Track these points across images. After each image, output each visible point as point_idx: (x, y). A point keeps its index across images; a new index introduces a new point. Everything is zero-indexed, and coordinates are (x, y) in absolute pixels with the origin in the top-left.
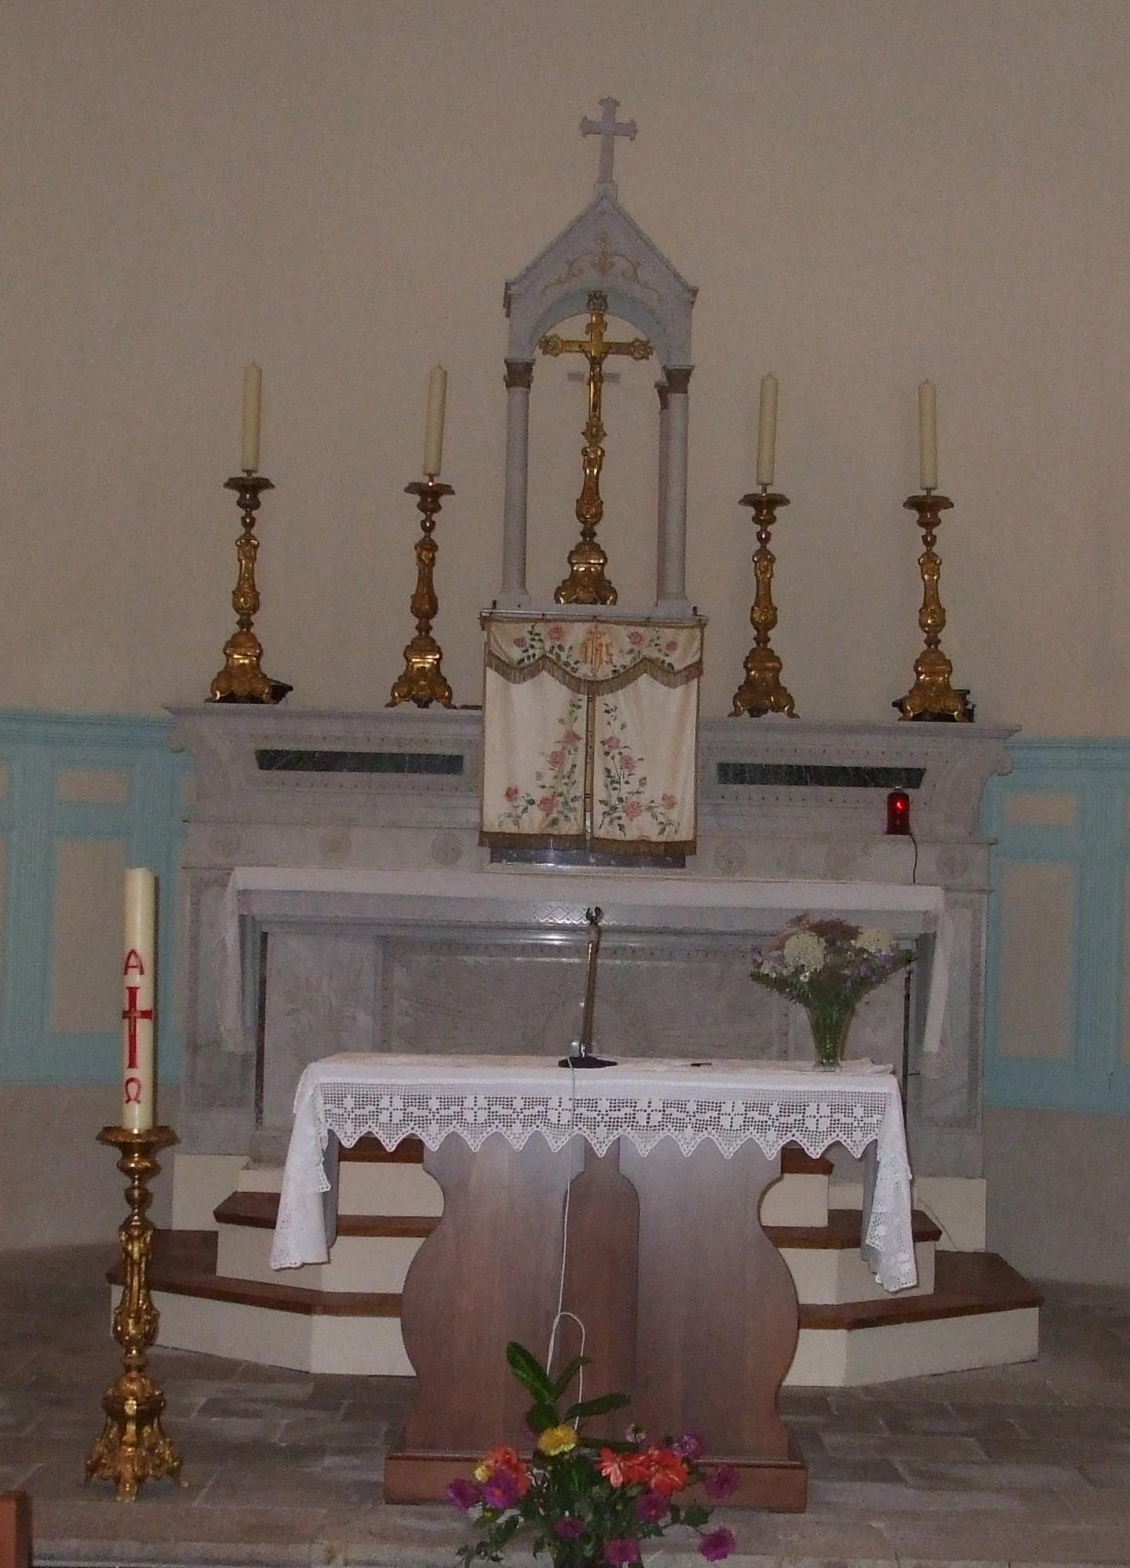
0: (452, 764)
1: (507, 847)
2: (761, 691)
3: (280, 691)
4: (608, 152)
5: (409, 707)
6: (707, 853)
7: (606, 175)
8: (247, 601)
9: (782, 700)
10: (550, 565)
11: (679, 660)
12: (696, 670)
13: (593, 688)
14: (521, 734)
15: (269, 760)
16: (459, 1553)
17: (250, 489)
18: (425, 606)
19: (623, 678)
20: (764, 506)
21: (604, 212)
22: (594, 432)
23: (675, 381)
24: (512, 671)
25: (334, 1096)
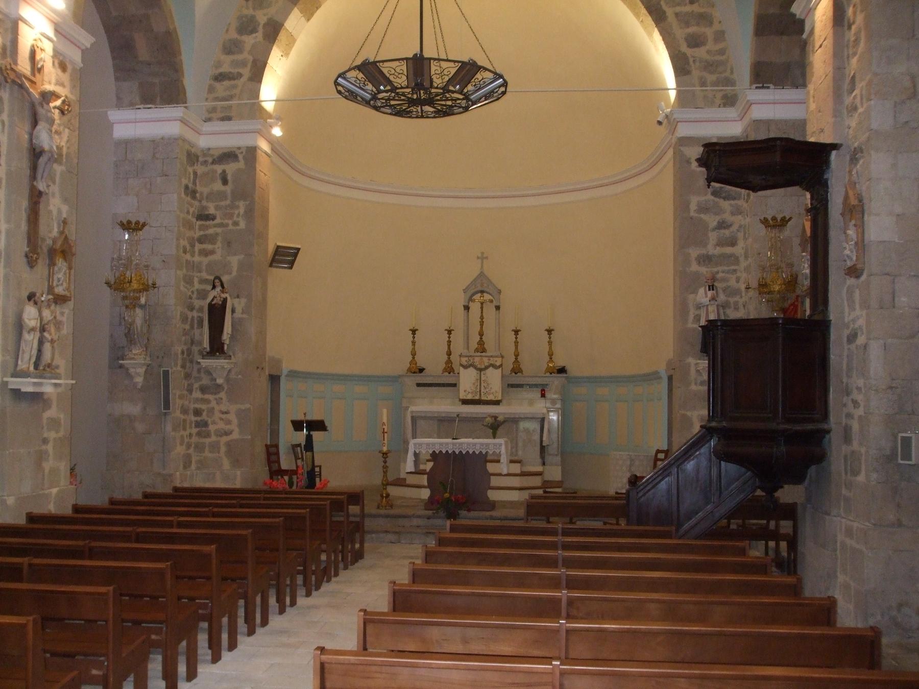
0: (455, 385)
1: (465, 402)
2: (517, 370)
3: (421, 370)
4: (482, 263)
5: (447, 374)
6: (504, 402)
7: (482, 267)
8: (414, 354)
9: (521, 371)
10: (474, 344)
11: (498, 364)
12: (501, 366)
13: (481, 370)
14: (467, 380)
15: (419, 385)
16: (43, 66)
17: (414, 331)
18: (449, 353)
19: (486, 368)
20: (516, 332)
21: (482, 275)
22: (482, 317)
23: (498, 308)
24: (465, 367)
25: (415, 444)
